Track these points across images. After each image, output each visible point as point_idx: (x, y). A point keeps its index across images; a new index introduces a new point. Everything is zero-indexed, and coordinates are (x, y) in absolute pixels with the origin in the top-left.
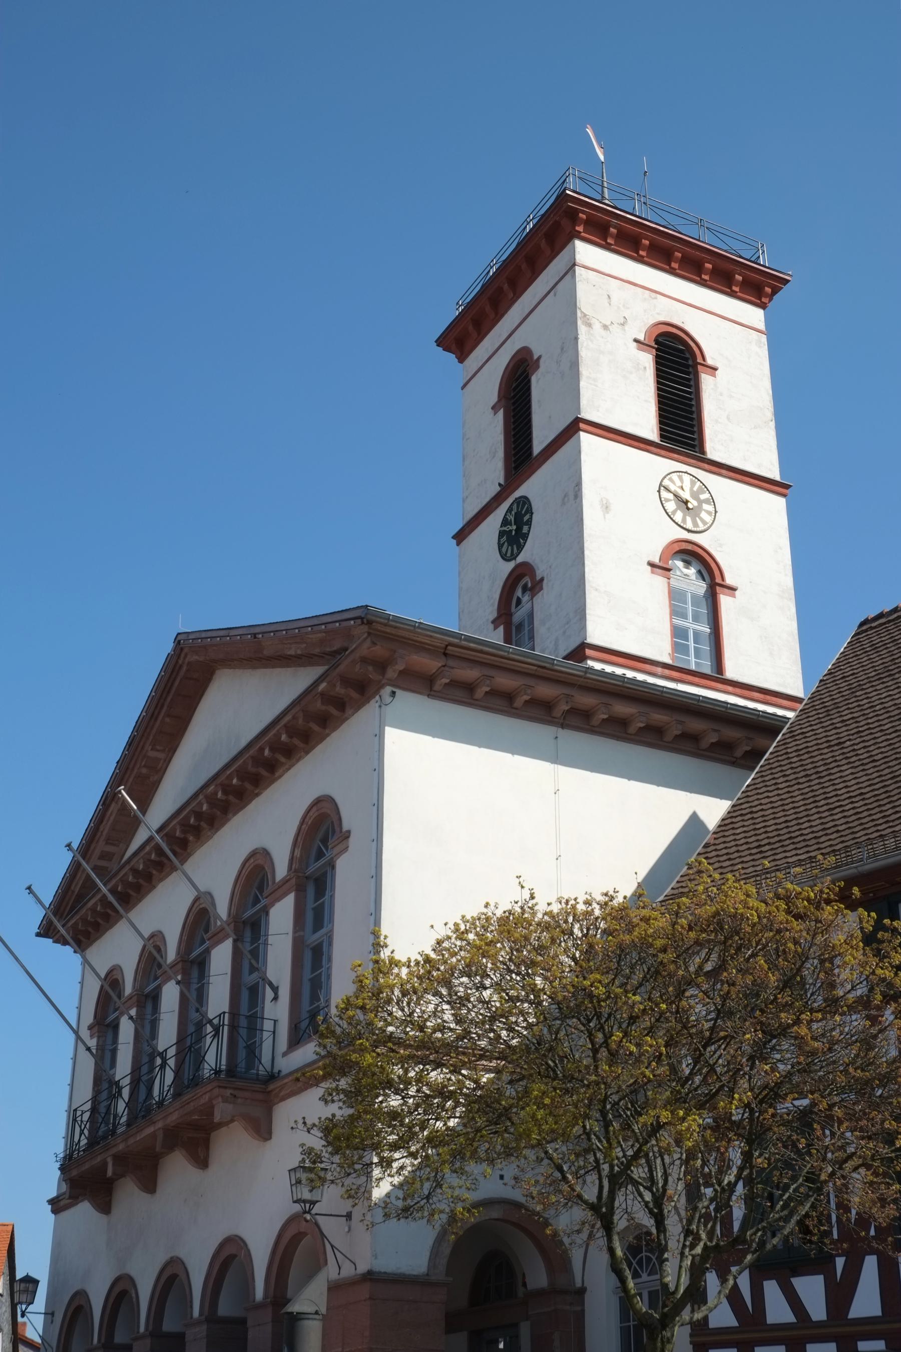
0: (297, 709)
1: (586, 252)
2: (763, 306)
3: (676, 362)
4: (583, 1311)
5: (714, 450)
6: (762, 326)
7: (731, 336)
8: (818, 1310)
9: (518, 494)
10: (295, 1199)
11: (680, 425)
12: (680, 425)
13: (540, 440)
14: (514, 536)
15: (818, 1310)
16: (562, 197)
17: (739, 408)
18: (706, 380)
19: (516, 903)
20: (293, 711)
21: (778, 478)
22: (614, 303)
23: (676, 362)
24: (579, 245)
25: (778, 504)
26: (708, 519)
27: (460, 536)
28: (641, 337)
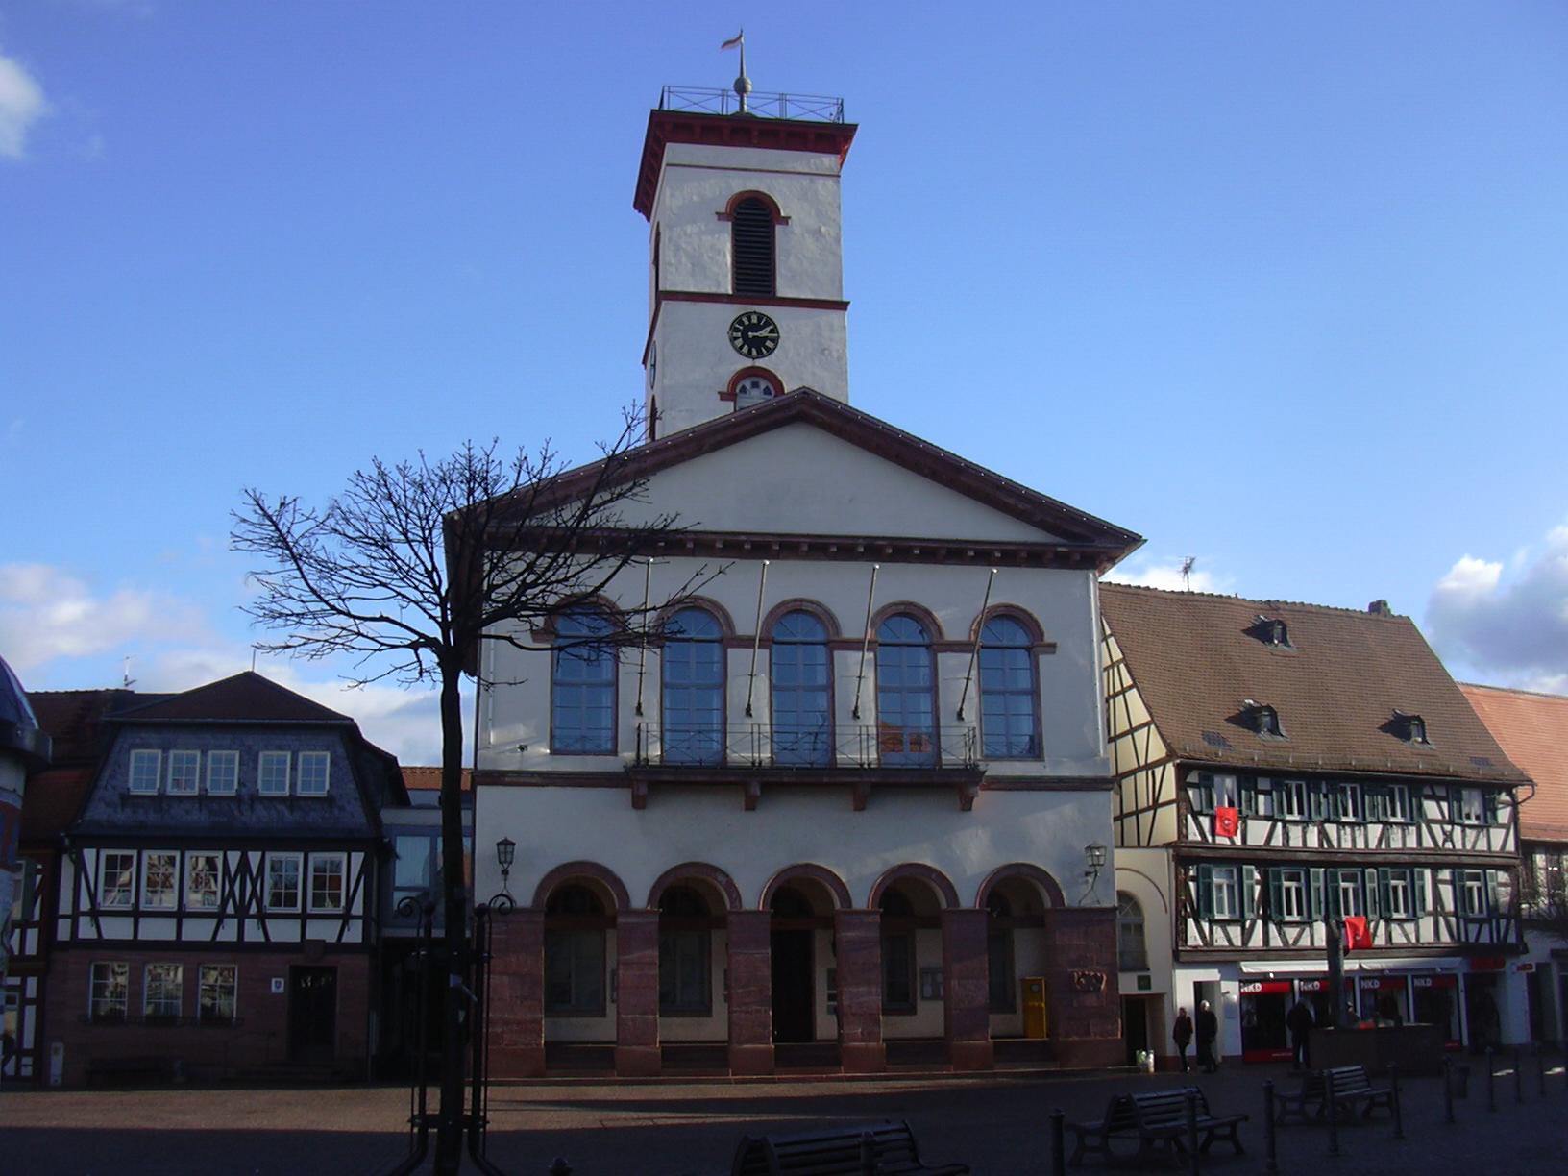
5: (783, 290)
18: (779, 228)
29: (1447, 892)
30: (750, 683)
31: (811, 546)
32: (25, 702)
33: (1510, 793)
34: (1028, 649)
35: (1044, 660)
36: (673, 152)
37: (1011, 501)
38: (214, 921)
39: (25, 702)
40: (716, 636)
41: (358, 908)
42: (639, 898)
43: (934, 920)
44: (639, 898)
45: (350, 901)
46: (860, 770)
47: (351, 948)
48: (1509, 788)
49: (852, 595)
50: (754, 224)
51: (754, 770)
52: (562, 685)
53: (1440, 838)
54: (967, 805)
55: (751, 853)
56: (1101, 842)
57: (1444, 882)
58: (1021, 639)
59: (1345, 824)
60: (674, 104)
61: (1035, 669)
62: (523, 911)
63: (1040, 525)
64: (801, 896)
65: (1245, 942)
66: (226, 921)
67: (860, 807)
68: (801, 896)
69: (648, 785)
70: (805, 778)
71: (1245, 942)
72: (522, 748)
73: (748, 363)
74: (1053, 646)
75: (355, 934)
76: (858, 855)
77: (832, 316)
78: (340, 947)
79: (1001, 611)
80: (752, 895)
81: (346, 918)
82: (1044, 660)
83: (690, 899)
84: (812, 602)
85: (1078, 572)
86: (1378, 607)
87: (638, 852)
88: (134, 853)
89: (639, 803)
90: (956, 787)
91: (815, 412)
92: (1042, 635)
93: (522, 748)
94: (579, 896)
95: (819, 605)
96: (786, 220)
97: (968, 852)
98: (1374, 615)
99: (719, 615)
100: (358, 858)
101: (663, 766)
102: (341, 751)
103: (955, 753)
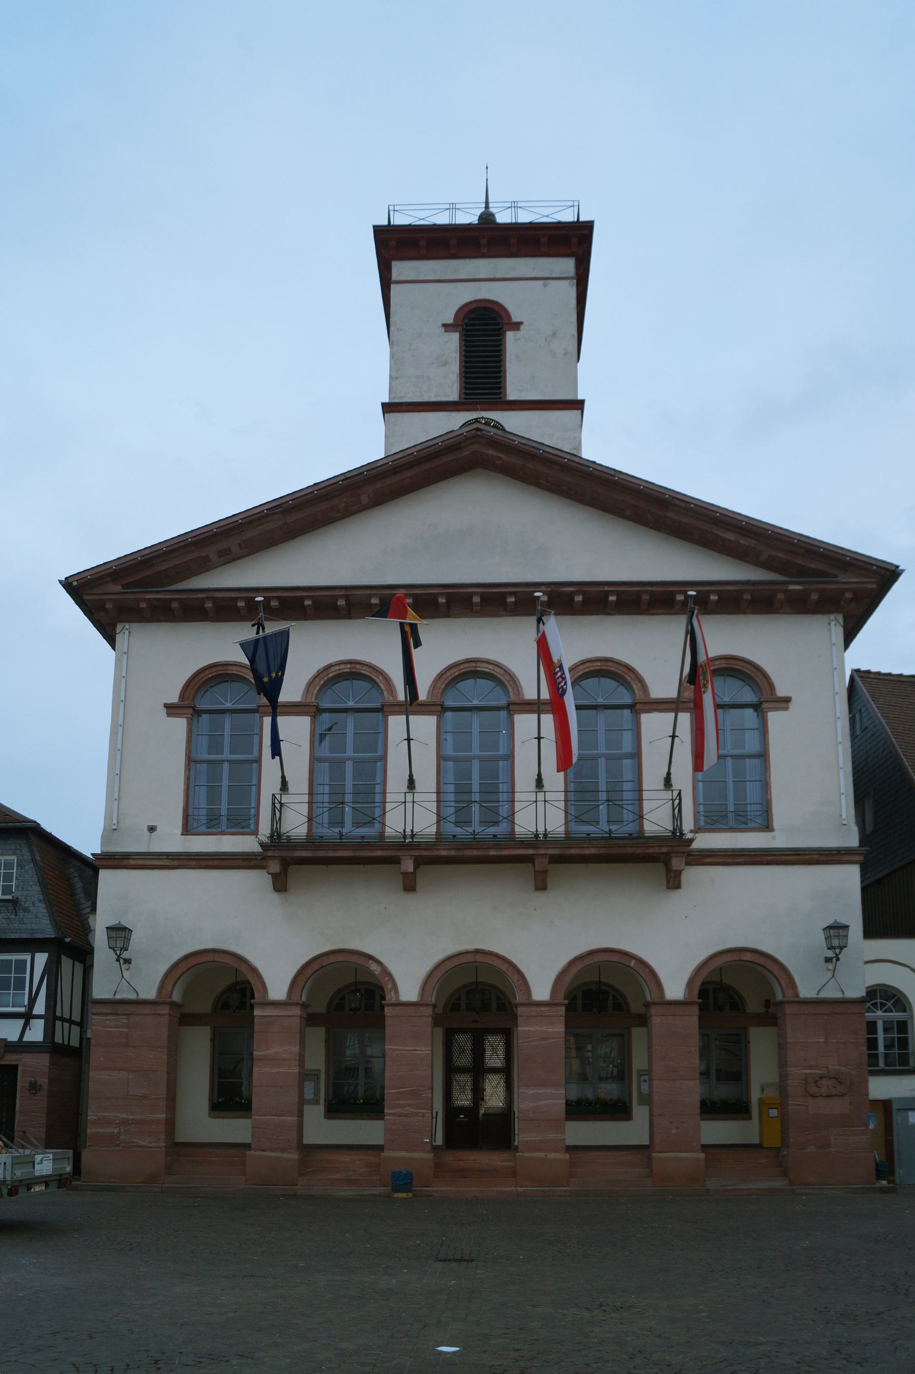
0: (343, 593)
5: (512, 394)
18: (510, 336)
20: (743, 587)
30: (413, 748)
31: (483, 596)
34: (757, 707)
35: (775, 718)
36: (400, 269)
37: (731, 536)
38: (21, 1022)
40: (627, 699)
41: (40, 1008)
42: (541, 991)
43: (770, 1016)
44: (541, 991)
45: (32, 1001)
46: (538, 841)
47: (32, 1047)
50: (483, 334)
51: (409, 844)
54: (674, 882)
55: (410, 943)
56: (843, 921)
58: (748, 695)
60: (399, 220)
61: (763, 730)
62: (146, 1003)
63: (766, 565)
66: (33, 1022)
67: (541, 886)
69: (288, 863)
70: (476, 849)
72: (152, 829)
74: (787, 700)
75: (36, 1033)
76: (541, 941)
77: (569, 415)
78: (21, 1046)
79: (722, 664)
81: (28, 1017)
82: (775, 718)
83: (347, 995)
84: (488, 662)
85: (818, 617)
88: (27, 957)
89: (280, 885)
90: (662, 860)
91: (491, 452)
92: (772, 687)
93: (152, 829)
94: (219, 992)
95: (497, 665)
96: (517, 326)
97: (672, 938)
99: (379, 680)
100: (41, 959)
101: (311, 841)
102: (27, 855)
103: (657, 819)
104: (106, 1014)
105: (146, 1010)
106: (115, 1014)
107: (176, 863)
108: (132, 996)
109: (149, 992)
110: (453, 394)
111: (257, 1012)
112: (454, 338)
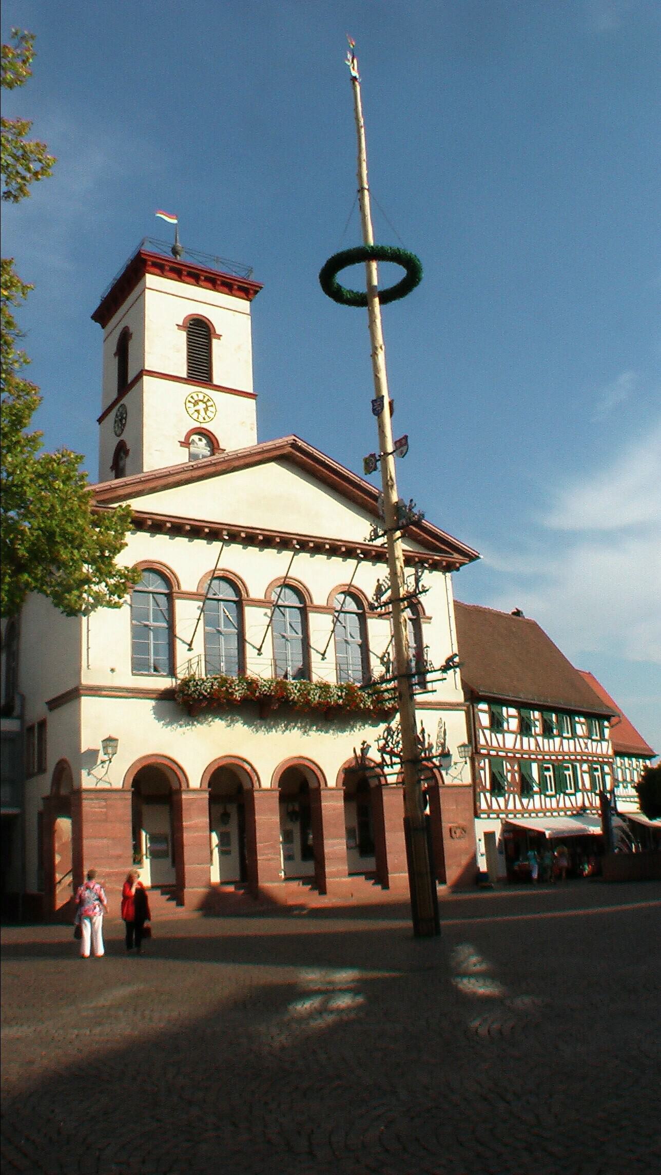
1: (151, 280)
2: (250, 301)
3: (200, 333)
4: (205, 645)
5: (216, 381)
6: (178, 640)
7: (231, 318)
8: (503, 807)
9: (122, 402)
10: (191, 661)
11: (200, 369)
12: (200, 369)
13: (130, 378)
14: (121, 421)
15: (503, 807)
16: (139, 254)
17: (233, 358)
19: (19, 305)
21: (251, 391)
22: (166, 306)
23: (200, 333)
24: (148, 277)
25: (252, 402)
26: (212, 415)
27: (100, 420)
28: (181, 324)
29: (586, 777)
32: (262, 445)
33: (609, 721)
39: (262, 445)
42: (332, 782)
48: (608, 718)
49: (258, 569)
52: (214, 611)
53: (583, 746)
55: (265, 751)
57: (585, 772)
59: (565, 738)
64: (298, 782)
65: (506, 806)
68: (298, 782)
71: (506, 806)
73: (197, 425)
74: (430, 618)
80: (267, 778)
83: (230, 786)
86: (518, 613)
87: (197, 749)
93: (112, 670)
94: (155, 785)
98: (514, 617)
104: (92, 799)
105: (117, 796)
106: (97, 799)
107: (130, 694)
108: (107, 786)
109: (118, 784)
110: (183, 373)
111: (184, 796)
112: (184, 334)
